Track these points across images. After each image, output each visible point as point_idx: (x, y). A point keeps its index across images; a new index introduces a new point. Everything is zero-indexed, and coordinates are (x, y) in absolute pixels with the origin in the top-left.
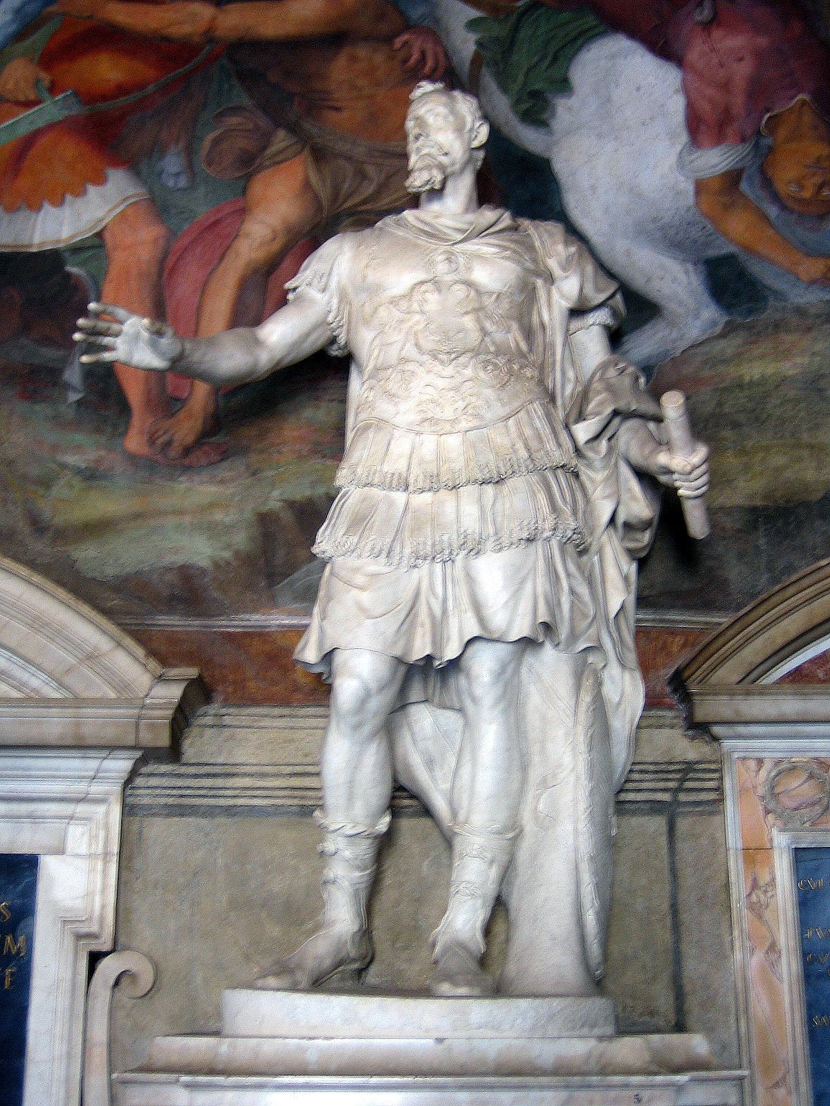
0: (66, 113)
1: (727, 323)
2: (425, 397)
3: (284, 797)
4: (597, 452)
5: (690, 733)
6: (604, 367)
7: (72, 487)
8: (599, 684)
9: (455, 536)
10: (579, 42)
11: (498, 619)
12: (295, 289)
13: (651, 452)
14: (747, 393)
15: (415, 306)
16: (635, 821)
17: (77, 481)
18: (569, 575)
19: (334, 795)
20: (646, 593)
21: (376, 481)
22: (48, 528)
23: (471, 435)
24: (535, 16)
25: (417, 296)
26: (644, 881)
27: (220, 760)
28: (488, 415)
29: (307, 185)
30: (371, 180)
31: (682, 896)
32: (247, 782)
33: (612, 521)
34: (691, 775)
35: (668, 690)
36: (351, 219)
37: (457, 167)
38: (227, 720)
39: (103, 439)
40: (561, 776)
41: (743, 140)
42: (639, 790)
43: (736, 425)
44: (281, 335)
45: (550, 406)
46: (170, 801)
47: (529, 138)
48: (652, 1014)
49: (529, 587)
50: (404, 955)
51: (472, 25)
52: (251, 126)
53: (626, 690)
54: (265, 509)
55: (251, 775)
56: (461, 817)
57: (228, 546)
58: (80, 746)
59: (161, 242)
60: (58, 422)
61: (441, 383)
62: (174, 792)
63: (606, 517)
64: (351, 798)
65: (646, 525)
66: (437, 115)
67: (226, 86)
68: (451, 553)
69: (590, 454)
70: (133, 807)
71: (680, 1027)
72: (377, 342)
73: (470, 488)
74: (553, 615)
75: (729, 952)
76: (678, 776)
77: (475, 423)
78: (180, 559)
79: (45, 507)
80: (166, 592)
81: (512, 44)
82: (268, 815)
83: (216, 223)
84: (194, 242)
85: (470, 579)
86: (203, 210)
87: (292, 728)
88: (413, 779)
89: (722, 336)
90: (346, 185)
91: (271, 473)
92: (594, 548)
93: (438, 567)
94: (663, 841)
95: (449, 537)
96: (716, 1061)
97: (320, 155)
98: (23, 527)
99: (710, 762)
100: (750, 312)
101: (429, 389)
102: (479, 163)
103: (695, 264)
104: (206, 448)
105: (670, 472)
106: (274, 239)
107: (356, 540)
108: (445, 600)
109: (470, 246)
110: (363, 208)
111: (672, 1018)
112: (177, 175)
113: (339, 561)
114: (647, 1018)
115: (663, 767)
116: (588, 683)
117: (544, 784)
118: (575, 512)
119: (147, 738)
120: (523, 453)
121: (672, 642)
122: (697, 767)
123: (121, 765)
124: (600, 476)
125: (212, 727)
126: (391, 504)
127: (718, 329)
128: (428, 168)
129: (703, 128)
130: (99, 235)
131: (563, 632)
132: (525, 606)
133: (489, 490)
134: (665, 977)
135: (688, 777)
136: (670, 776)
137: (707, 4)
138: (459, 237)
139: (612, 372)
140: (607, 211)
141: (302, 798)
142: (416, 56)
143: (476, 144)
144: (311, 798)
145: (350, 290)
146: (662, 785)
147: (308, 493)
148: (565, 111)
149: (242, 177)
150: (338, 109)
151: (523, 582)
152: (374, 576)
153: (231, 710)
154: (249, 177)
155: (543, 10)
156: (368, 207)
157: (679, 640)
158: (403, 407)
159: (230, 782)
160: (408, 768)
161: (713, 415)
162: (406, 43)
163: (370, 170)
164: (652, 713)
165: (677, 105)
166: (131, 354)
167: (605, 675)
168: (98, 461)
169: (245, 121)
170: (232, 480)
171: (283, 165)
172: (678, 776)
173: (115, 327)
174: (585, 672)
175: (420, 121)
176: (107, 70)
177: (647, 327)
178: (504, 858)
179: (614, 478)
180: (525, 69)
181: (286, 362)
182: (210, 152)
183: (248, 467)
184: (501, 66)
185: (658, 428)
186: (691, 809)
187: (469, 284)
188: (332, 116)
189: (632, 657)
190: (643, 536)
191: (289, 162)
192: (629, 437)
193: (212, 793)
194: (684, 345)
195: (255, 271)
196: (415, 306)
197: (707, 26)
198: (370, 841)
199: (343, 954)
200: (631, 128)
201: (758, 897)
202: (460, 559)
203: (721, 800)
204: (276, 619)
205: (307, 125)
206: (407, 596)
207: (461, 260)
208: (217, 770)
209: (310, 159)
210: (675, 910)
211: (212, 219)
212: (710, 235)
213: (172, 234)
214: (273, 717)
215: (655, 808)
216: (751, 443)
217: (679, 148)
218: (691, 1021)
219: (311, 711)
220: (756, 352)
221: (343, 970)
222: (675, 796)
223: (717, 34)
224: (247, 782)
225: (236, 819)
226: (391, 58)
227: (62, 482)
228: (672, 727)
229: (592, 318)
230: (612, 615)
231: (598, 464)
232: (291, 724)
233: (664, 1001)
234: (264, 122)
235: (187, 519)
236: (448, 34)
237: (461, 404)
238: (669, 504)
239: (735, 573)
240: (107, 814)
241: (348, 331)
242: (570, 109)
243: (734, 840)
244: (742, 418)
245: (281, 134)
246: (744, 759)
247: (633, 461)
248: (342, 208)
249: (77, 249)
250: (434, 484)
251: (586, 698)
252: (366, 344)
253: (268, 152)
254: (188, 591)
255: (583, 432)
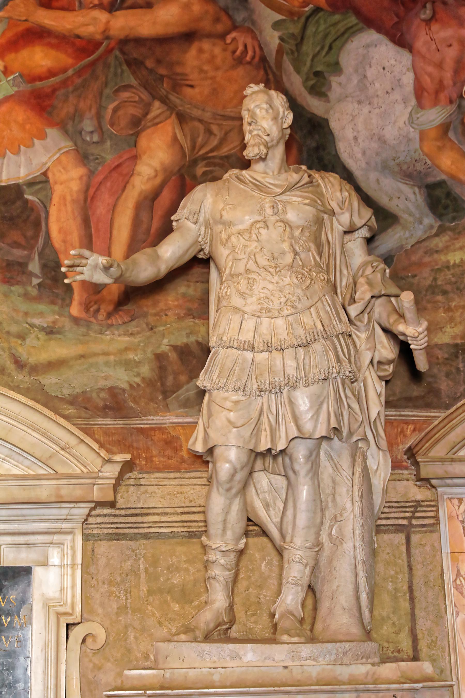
0: (16, 89)
1: (440, 226)
2: (262, 295)
3: (178, 527)
4: (361, 321)
5: (418, 483)
6: (364, 265)
7: (38, 339)
8: (365, 459)
9: (282, 379)
10: (346, 36)
11: (308, 427)
12: (177, 221)
13: (395, 321)
14: (452, 271)
15: (254, 237)
16: (386, 537)
17: (42, 336)
18: (346, 397)
19: (215, 528)
20: (391, 399)
21: (235, 345)
22: (25, 366)
23: (290, 318)
24: (317, 18)
25: (254, 231)
26: (392, 573)
27: (139, 506)
28: (299, 306)
29: (175, 139)
30: (215, 135)
31: (415, 582)
32: (156, 518)
33: (372, 362)
34: (419, 509)
35: (405, 457)
36: (204, 162)
37: (275, 142)
38: (143, 482)
39: (56, 308)
40: (345, 515)
41: (451, 102)
42: (389, 518)
43: (445, 293)
44: (171, 252)
45: (335, 296)
46: (110, 531)
47: (315, 105)
48: (399, 651)
49: (325, 406)
50: (252, 619)
51: (276, 25)
52: (137, 99)
53: (379, 463)
54: (159, 351)
55: (158, 514)
56: (288, 539)
57: (138, 375)
58: (60, 502)
59: (85, 179)
60: (26, 296)
61: (271, 287)
62: (113, 526)
63: (368, 361)
64: (224, 530)
65: (389, 362)
66: (262, 109)
67: (119, 71)
68: (280, 388)
69: (358, 323)
70: (87, 535)
71: (415, 658)
72: (231, 257)
73: (290, 349)
74: (339, 424)
75: (444, 614)
76: (412, 509)
77: (293, 311)
78: (109, 383)
79: (22, 352)
80: (101, 404)
81: (302, 39)
82: (170, 537)
83: (119, 166)
84: (106, 178)
85: (291, 403)
86: (110, 157)
87: (181, 485)
88: (257, 515)
89: (437, 235)
90: (200, 139)
91: (162, 328)
92: (361, 379)
93: (273, 396)
94: (404, 548)
95: (279, 379)
96: (437, 677)
97: (182, 118)
98: (10, 366)
99: (431, 501)
100: (454, 219)
101: (265, 291)
102: (287, 136)
103: (420, 188)
104: (121, 313)
105: (404, 334)
106: (156, 176)
107: (225, 381)
108: (277, 415)
109: (283, 198)
110: (210, 155)
111: (411, 653)
112: (92, 132)
113: (215, 393)
114: (396, 654)
115: (403, 504)
116: (359, 461)
117: (335, 519)
118: (350, 361)
119: (97, 495)
120: (320, 327)
121: (407, 429)
122: (423, 504)
123: (81, 511)
124: (363, 336)
125: (134, 486)
126: (244, 360)
127: (434, 231)
128: (258, 145)
129: (425, 94)
130: (45, 174)
131: (345, 432)
132: (323, 417)
133: (301, 351)
134: (407, 629)
135: (418, 509)
136: (407, 510)
137: (429, 6)
138: (279, 191)
139: (369, 271)
140: (364, 153)
141: (189, 527)
142: (241, 48)
143: (285, 126)
144: (194, 527)
145: (211, 221)
146: (402, 515)
147: (185, 340)
148: (337, 85)
149: (132, 135)
150: (192, 86)
151: (322, 403)
152: (237, 402)
153: (145, 475)
154: (137, 135)
155: (321, 14)
156: (214, 154)
157: (411, 427)
158: (249, 300)
159: (146, 519)
160: (253, 508)
161: (430, 286)
162: (234, 39)
163: (215, 128)
164: (396, 472)
165: (409, 79)
166: (92, 276)
167: (369, 453)
168: (54, 322)
169: (133, 95)
170: (138, 333)
171: (160, 125)
172: (412, 509)
173: (84, 261)
174: (356, 454)
175: (253, 115)
176: (40, 58)
177: (390, 230)
178: (312, 562)
179: (372, 338)
180: (311, 57)
181: (175, 267)
182: (111, 117)
183: (147, 324)
184: (296, 54)
185: (397, 302)
186: (419, 529)
187: (285, 222)
188: (188, 91)
189: (384, 444)
190: (390, 367)
191: (162, 124)
192: (380, 309)
193: (135, 525)
194: (413, 241)
195: (146, 198)
196: (254, 237)
197: (428, 22)
198: (235, 554)
199: (220, 620)
200: (379, 95)
201: (460, 581)
202: (285, 392)
203: (439, 524)
204: (169, 419)
205: (173, 98)
206: (255, 415)
207: (280, 207)
208: (138, 511)
209: (176, 121)
210: (411, 588)
211: (116, 163)
212: (430, 168)
213: (91, 173)
214: (170, 479)
215: (399, 529)
216: (453, 304)
217: (410, 109)
218: (422, 655)
219: (193, 474)
220: (458, 245)
221: (219, 630)
222: (410, 522)
223: (435, 27)
224: (156, 518)
225: (151, 540)
226: (225, 50)
227: (33, 336)
228: (408, 480)
229: (356, 234)
230: (372, 420)
231: (363, 328)
232: (181, 483)
233: (406, 644)
234: (145, 96)
235: (112, 358)
236: (261, 32)
237: (283, 300)
238: (405, 351)
239: (444, 385)
240: (73, 541)
241: (211, 245)
242: (340, 84)
243: (446, 548)
244: (448, 288)
245: (157, 104)
246: (450, 499)
247: (383, 325)
248: (197, 155)
249: (31, 184)
250: (268, 348)
251: (359, 469)
252: (222, 254)
253: (150, 116)
254: (115, 404)
255: (353, 310)
